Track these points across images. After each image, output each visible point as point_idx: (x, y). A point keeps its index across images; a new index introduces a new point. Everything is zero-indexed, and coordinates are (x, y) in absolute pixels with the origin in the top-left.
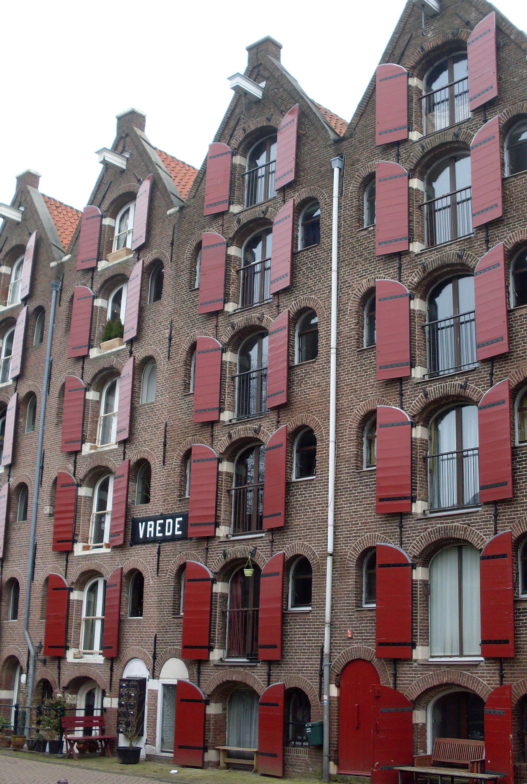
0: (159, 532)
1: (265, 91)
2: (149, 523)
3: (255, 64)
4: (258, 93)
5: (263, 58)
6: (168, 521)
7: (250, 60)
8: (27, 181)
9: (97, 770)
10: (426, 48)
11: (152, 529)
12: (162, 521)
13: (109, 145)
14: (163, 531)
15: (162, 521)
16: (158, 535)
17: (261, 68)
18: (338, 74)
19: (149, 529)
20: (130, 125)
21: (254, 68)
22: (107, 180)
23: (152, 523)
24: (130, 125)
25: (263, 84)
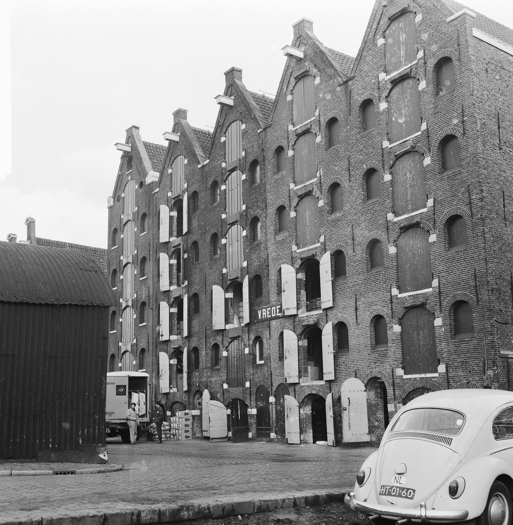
0: (279, 312)
1: (305, 53)
2: (263, 310)
3: (298, 36)
4: (301, 55)
5: (302, 34)
6: (273, 308)
7: (295, 33)
8: (180, 115)
9: (242, 463)
10: (389, 18)
11: (265, 314)
12: (270, 309)
13: (222, 92)
14: (270, 314)
15: (270, 309)
16: (268, 316)
17: (301, 38)
18: (343, 35)
19: (263, 314)
20: (232, 76)
21: (298, 38)
22: (302, 366)
23: (265, 310)
24: (232, 76)
25: (303, 49)
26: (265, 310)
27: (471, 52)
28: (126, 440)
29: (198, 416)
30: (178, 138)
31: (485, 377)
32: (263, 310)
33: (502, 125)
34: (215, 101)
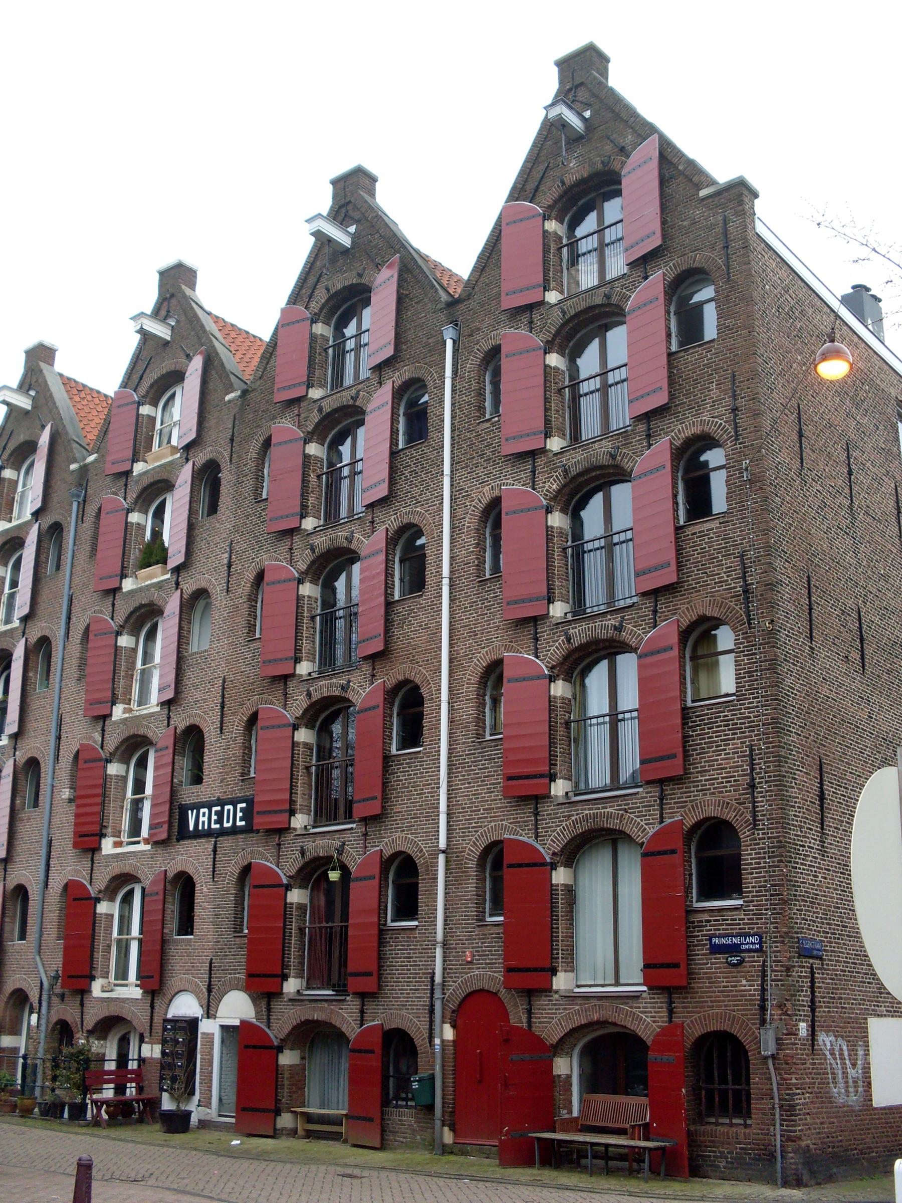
2: (202, 810)
5: (353, 194)
6: (227, 807)
7: (335, 196)
8: (40, 356)
11: (206, 819)
12: (219, 808)
14: (220, 821)
15: (219, 808)
16: (214, 826)
17: (350, 207)
19: (201, 819)
20: (176, 282)
23: (206, 810)
24: (176, 282)
25: (352, 229)
26: (206, 810)
27: (248, 794)
28: (347, 927)
29: (122, 776)
30: (30, 402)
31: (66, 1050)
32: (202, 810)
33: (808, 430)
34: (133, 326)
